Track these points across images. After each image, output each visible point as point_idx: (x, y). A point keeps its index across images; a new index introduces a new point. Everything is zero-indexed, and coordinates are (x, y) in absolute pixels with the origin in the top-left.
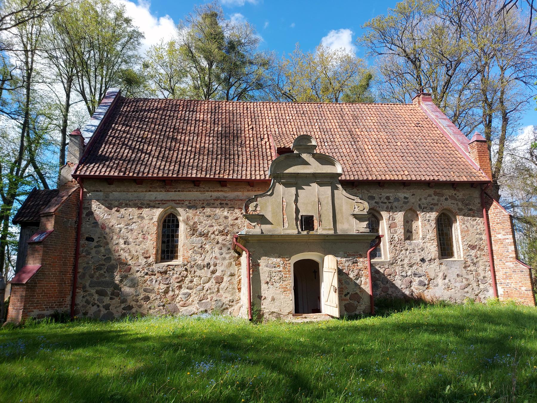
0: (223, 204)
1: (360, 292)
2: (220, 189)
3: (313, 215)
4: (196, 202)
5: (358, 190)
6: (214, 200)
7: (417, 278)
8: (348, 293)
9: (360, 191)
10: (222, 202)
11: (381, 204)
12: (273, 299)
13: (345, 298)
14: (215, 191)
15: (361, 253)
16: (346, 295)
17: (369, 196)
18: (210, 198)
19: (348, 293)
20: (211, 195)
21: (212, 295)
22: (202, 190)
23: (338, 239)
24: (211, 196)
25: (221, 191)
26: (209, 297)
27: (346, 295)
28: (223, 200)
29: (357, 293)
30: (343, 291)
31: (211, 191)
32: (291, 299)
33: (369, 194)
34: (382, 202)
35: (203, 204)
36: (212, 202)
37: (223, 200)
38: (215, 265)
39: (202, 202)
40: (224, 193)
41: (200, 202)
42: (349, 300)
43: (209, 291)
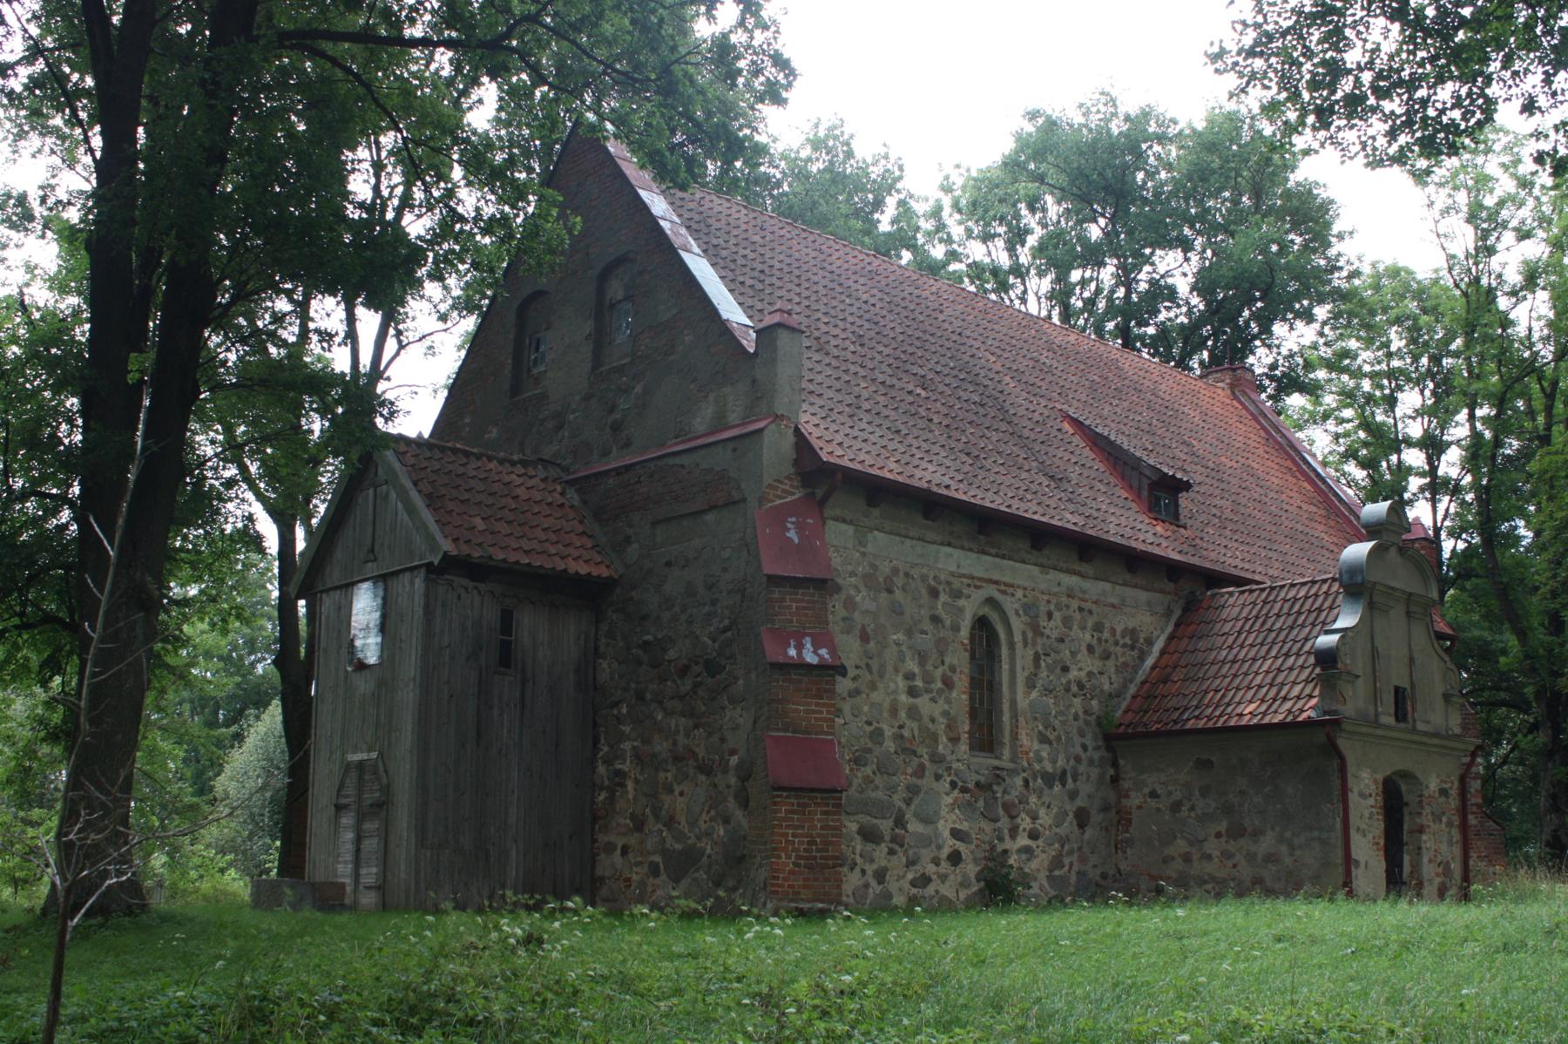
25: (1079, 574)
26: (1067, 861)
31: (1061, 570)
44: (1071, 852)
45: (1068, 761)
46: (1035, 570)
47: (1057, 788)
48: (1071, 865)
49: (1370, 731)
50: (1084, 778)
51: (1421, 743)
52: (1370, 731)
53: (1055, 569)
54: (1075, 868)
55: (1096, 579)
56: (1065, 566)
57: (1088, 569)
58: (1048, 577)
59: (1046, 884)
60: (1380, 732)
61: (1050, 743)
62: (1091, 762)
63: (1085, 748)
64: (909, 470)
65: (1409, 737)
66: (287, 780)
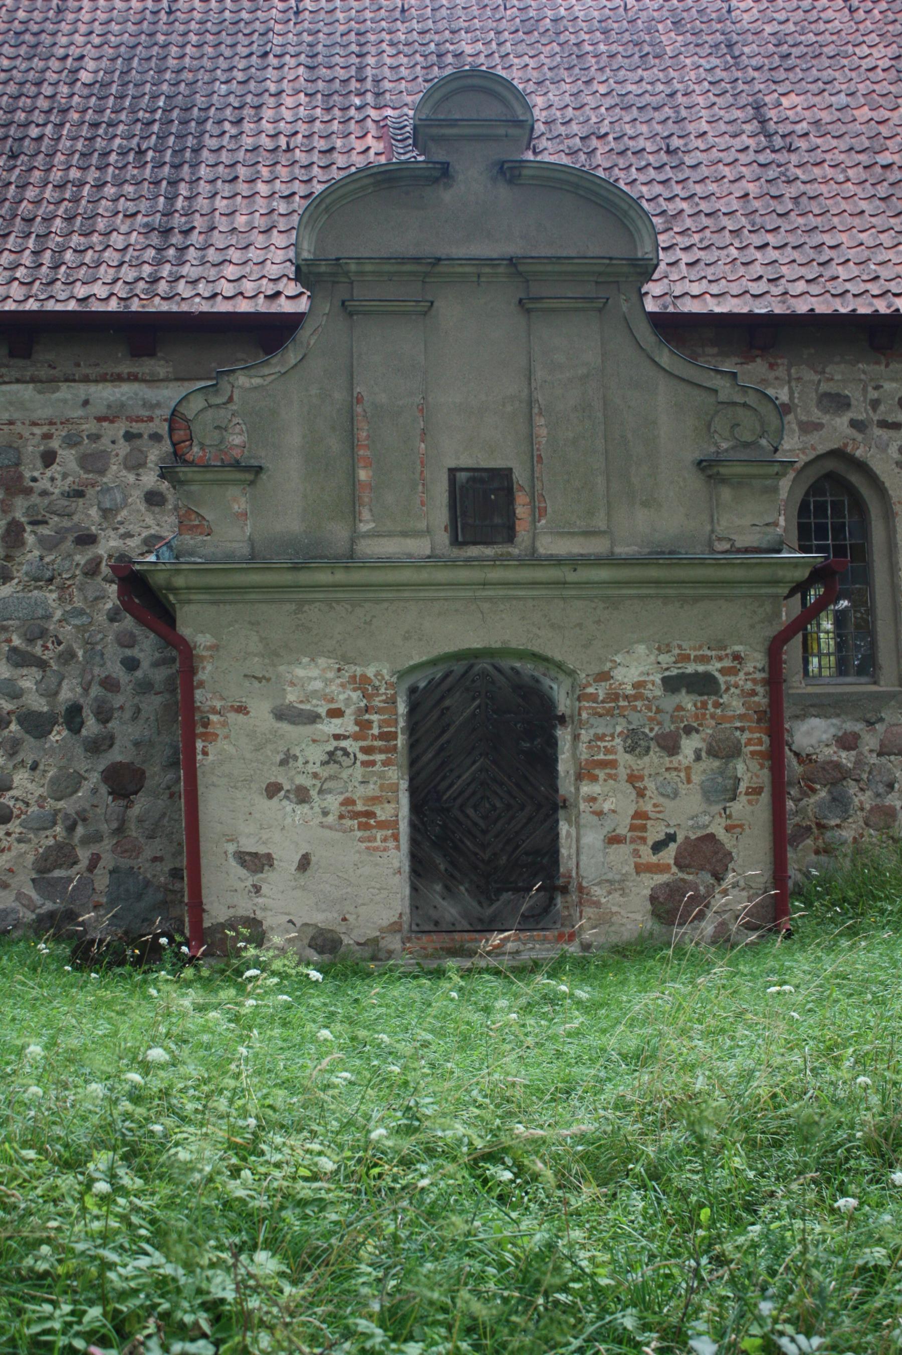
0: (140, 436)
1: (728, 829)
2: (124, 369)
3: (509, 464)
4: (18, 428)
5: (772, 366)
6: (100, 419)
7: (153, 697)
8: (671, 838)
9: (781, 372)
10: (136, 428)
11: (878, 432)
12: (304, 863)
13: (654, 859)
14: (103, 379)
15: (737, 648)
16: (658, 847)
17: (827, 395)
18: (80, 412)
19: (671, 838)
20: (83, 397)
21: (95, 849)
22: (43, 373)
23: (628, 583)
24: (86, 403)
25: (133, 378)
26: (83, 855)
27: (658, 847)
28: (139, 420)
29: (711, 837)
30: (644, 828)
31: (86, 380)
32: (396, 864)
33: (824, 387)
34: (884, 424)
35: (47, 436)
36: (90, 427)
37: (139, 420)
38: (104, 715)
39: (45, 429)
40: (143, 386)
41: (37, 431)
42: (674, 869)
43: (80, 830)
44: (94, 838)
45: (86, 690)
46: (27, 391)
47: (58, 735)
48: (95, 861)
49: (340, 576)
50: (127, 715)
51: (451, 584)
52: (340, 576)
53: (67, 380)
54: (108, 861)
55: (177, 379)
56: (92, 372)
57: (147, 366)
58: (57, 395)
59: (33, 894)
60: (357, 577)
61: (42, 664)
62: (145, 687)
63: (131, 665)
64: (81, 291)
65: (526, 574)
66: (684, 691)
